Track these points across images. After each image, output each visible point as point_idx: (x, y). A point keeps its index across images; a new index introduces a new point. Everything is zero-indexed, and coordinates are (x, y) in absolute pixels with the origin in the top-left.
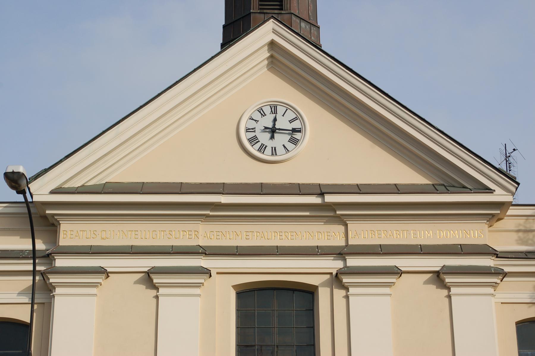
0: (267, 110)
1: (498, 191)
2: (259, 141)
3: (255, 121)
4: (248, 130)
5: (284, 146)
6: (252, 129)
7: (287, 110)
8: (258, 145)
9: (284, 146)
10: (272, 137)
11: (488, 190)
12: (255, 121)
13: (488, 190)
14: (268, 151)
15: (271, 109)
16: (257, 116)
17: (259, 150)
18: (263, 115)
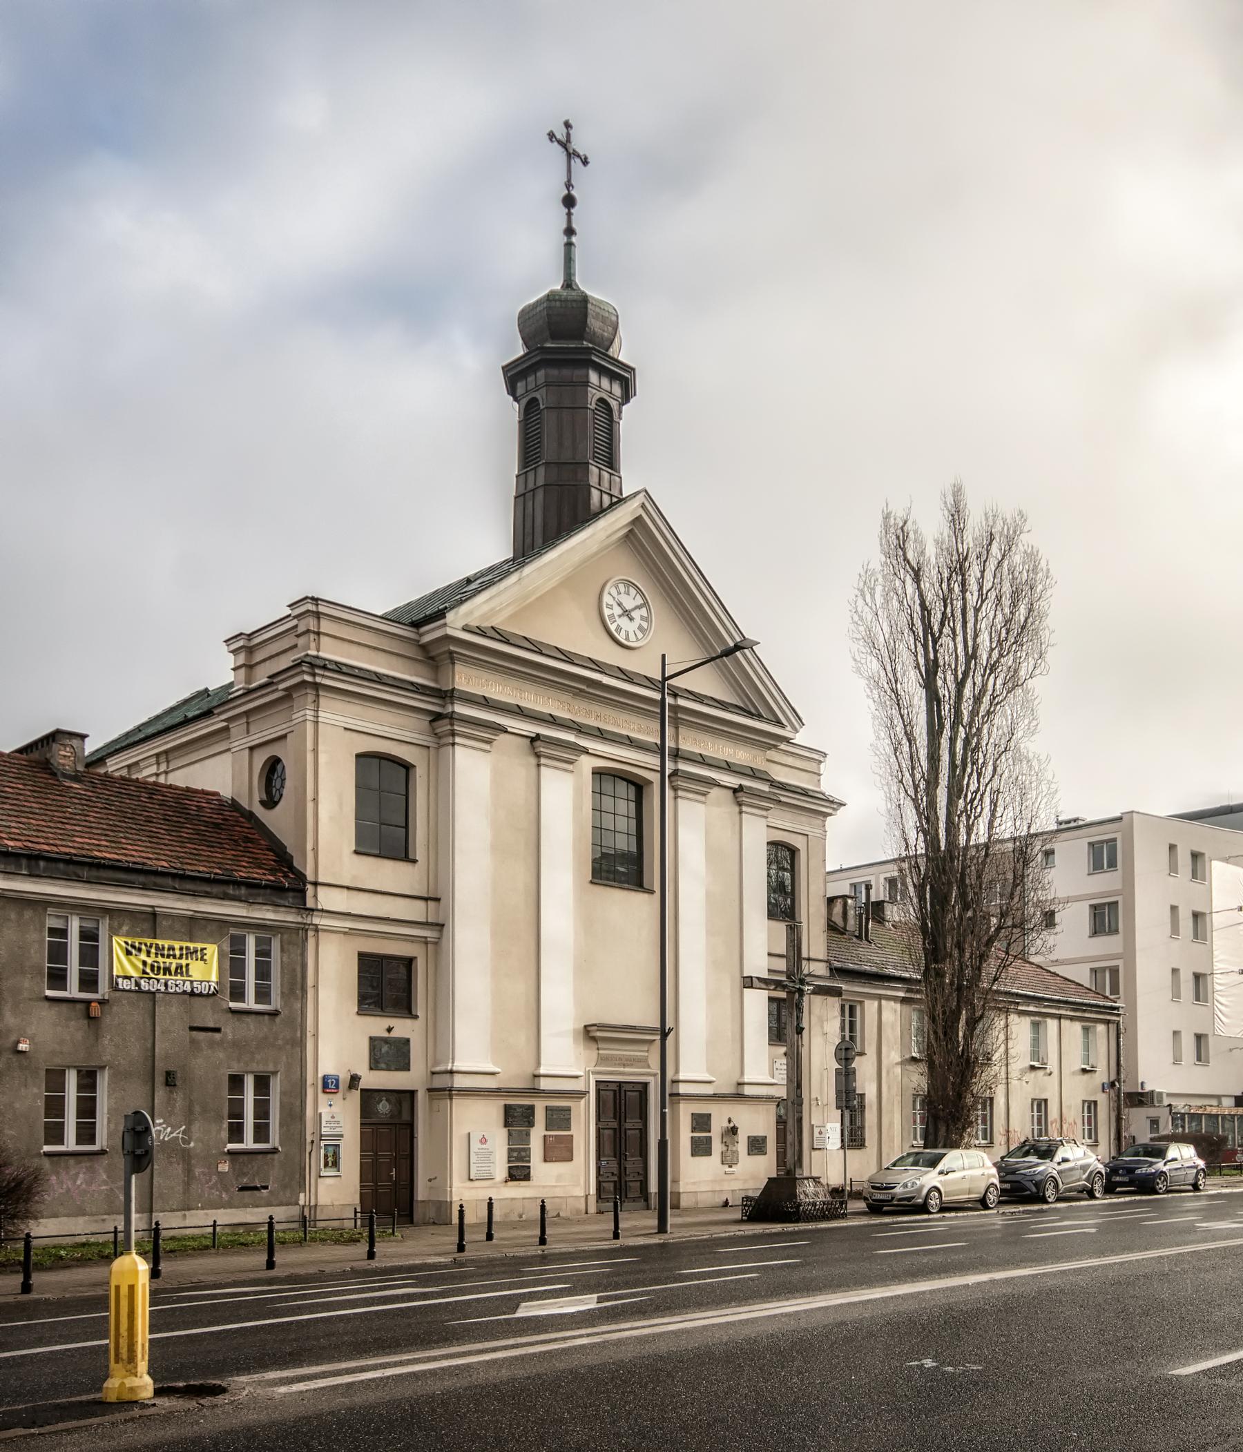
1: (789, 728)
5: (664, 656)
7: (855, 886)
9: (664, 656)
10: (631, 619)
11: (779, 723)
13: (779, 723)
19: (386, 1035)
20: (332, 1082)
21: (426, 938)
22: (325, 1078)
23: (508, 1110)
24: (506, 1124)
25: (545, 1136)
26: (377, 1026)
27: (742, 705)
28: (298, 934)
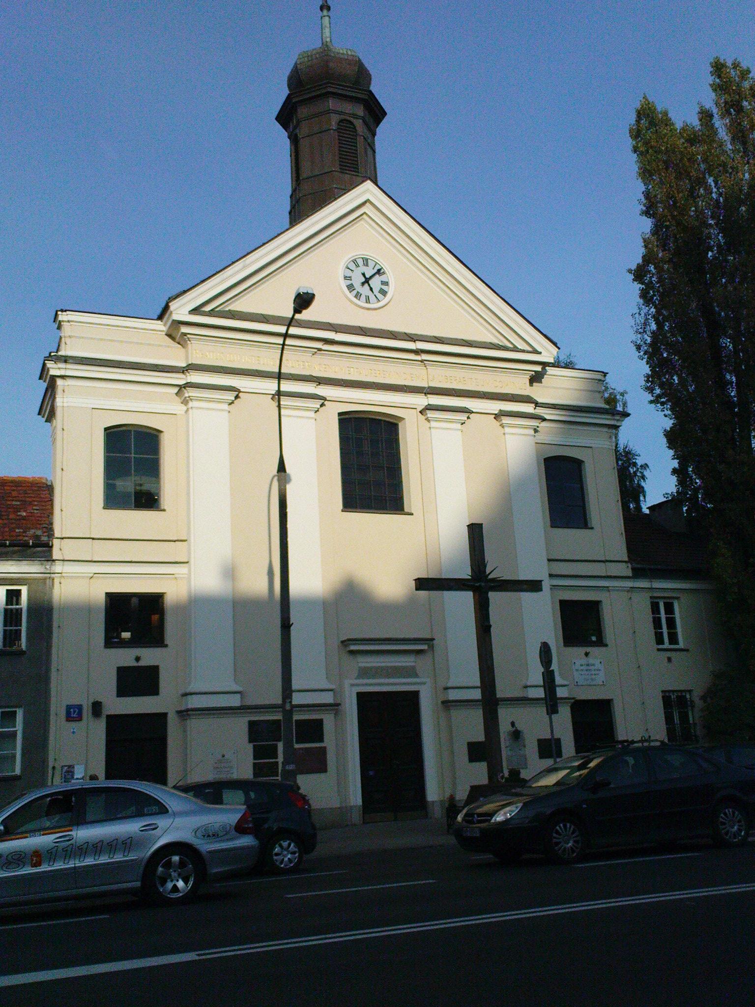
0: (360, 262)
2: (355, 289)
3: (352, 270)
4: (346, 278)
6: (349, 277)
8: (355, 292)
12: (352, 270)
14: (363, 298)
15: (364, 262)
16: (352, 266)
17: (356, 296)
18: (357, 266)
19: (135, 664)
20: (74, 712)
21: (607, 587)
22: (69, 708)
23: (252, 725)
24: (251, 741)
25: (254, 763)
26: (126, 657)
27: (495, 341)
28: (45, 583)
